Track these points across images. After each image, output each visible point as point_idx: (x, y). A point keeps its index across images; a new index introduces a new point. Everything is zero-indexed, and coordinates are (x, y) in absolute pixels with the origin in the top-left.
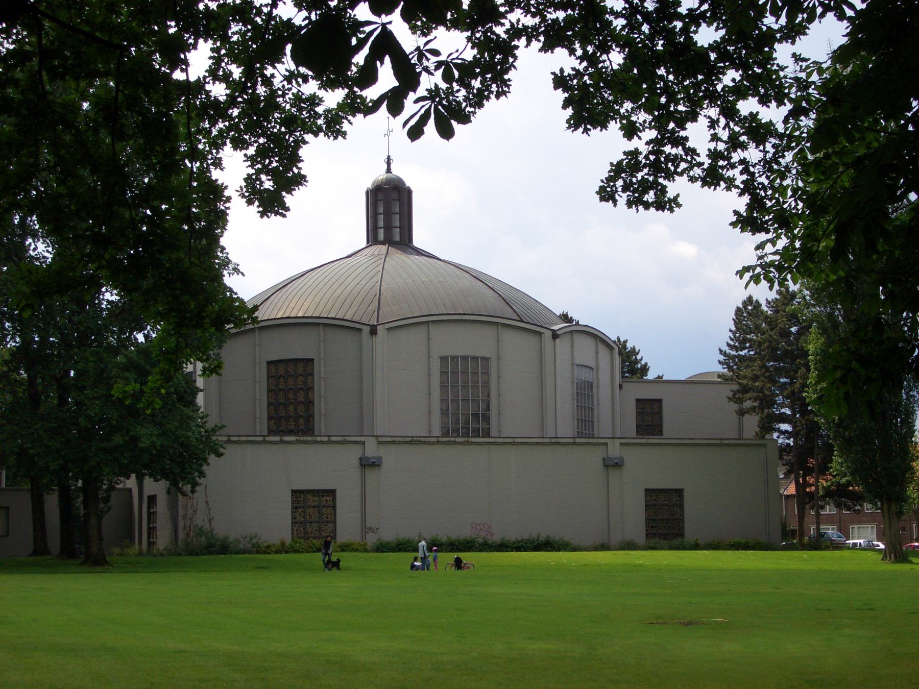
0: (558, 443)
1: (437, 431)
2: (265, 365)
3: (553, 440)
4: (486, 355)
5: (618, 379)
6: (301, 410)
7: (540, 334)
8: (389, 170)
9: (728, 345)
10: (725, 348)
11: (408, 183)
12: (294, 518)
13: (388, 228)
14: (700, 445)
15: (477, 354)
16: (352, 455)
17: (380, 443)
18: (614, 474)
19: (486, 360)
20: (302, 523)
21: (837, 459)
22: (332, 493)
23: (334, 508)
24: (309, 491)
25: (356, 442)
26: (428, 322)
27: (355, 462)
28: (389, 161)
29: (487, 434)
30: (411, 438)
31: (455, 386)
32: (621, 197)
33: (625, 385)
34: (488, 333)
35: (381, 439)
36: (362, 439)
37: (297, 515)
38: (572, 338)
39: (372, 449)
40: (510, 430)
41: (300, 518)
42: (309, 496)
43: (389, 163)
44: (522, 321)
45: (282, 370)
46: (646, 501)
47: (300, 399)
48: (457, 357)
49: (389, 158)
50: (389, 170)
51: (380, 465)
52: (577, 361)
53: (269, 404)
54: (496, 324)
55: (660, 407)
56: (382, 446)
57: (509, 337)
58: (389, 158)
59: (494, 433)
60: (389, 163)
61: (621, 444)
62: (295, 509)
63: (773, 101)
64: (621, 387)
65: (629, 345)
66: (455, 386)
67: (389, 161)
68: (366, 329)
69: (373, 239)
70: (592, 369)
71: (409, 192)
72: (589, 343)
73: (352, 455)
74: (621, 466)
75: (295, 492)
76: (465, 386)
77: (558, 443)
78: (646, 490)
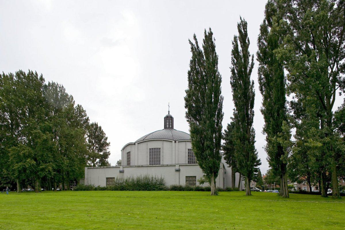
0: (163, 166)
1: (148, 164)
3: (162, 165)
7: (172, 142)
8: (169, 114)
11: (173, 116)
13: (169, 125)
14: (185, 165)
19: (160, 149)
24: (110, 178)
28: (169, 112)
29: (159, 164)
30: (104, 167)
32: (60, 85)
36: (120, 166)
40: (165, 163)
43: (169, 112)
45: (191, 179)
46: (186, 179)
48: (155, 148)
49: (169, 111)
50: (169, 114)
54: (185, 141)
57: (165, 143)
58: (169, 111)
59: (161, 163)
60: (169, 112)
62: (107, 182)
63: (334, 113)
67: (169, 112)
69: (165, 127)
74: (123, 172)
75: (107, 178)
77: (163, 166)
78: (186, 177)
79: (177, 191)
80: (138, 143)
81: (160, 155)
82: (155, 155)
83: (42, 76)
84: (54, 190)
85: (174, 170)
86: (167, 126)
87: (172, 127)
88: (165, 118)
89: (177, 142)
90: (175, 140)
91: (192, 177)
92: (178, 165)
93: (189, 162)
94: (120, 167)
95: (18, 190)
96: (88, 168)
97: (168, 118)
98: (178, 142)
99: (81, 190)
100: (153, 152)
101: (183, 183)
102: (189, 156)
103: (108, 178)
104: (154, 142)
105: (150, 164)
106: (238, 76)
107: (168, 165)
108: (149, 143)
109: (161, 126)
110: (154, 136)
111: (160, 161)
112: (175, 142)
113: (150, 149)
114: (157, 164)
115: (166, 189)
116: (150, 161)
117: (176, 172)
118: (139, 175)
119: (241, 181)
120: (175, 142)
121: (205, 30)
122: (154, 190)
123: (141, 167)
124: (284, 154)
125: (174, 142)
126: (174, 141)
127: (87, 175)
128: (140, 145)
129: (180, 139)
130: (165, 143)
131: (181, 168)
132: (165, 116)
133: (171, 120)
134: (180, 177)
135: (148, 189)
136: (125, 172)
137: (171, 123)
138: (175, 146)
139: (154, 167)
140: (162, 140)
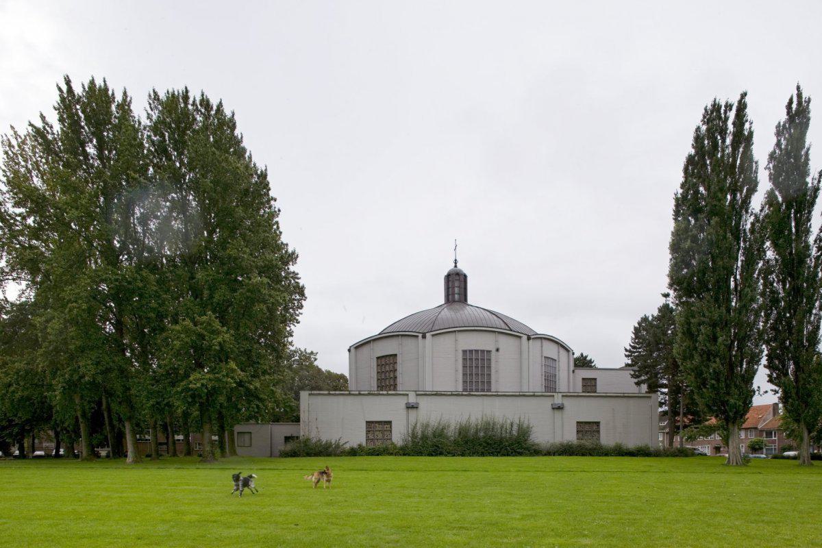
0: (524, 396)
1: (461, 389)
2: (375, 360)
4: (490, 349)
5: (572, 367)
6: (392, 383)
7: (520, 337)
8: (456, 266)
9: (630, 345)
10: (628, 348)
12: (367, 437)
15: (478, 348)
16: (401, 402)
17: (417, 395)
18: (557, 413)
20: (372, 439)
21: (748, 226)
22: (390, 423)
23: (391, 431)
25: (403, 395)
26: (455, 331)
27: (404, 406)
29: (489, 390)
31: (471, 367)
33: (576, 371)
34: (491, 337)
35: (418, 393)
37: (370, 435)
38: (542, 342)
39: (412, 399)
41: (371, 437)
42: (377, 425)
43: (456, 263)
44: (511, 330)
45: (587, 428)
47: (392, 376)
49: (456, 260)
50: (456, 266)
51: (417, 408)
52: (545, 355)
53: (378, 379)
55: (596, 383)
56: (418, 397)
58: (456, 260)
60: (456, 263)
61: (563, 396)
62: (368, 432)
64: (573, 371)
65: (588, 358)
66: (471, 367)
68: (420, 335)
70: (555, 360)
71: (465, 276)
72: (554, 347)
73: (401, 402)
74: (417, 408)
76: (477, 367)
78: (577, 422)
79: (576, 455)
81: (489, 367)
82: (477, 367)
84: (23, 456)
85: (550, 407)
89: (428, 335)
91: (589, 423)
92: (560, 395)
93: (378, 387)
94: (650, 397)
95: (130, 454)
96: (310, 395)
99: (308, 455)
101: (570, 436)
103: (373, 422)
104: (475, 334)
105: (465, 390)
106: (705, 190)
107: (536, 394)
108: (461, 337)
109: (436, 296)
111: (489, 383)
113: (464, 352)
115: (536, 451)
116: (465, 382)
117: (556, 411)
118: (463, 419)
120: (424, 337)
121: (83, 85)
122: (520, 454)
123: (449, 395)
125: (525, 337)
126: (526, 337)
127: (307, 414)
130: (409, 343)
131: (568, 403)
135: (503, 451)
136: (421, 406)
139: (430, 397)
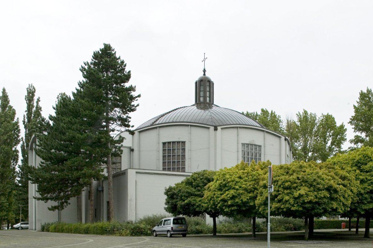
8: (204, 74)
19: (184, 143)
28: (204, 71)
48: (179, 142)
50: (204, 74)
54: (237, 127)
67: (204, 71)
80: (140, 132)
83: (126, 64)
86: (202, 99)
87: (210, 101)
88: (196, 83)
89: (219, 128)
90: (215, 125)
97: (202, 82)
98: (222, 129)
100: (169, 150)
102: (164, 157)
108: (163, 131)
110: (176, 118)
112: (216, 129)
113: (164, 144)
114: (174, 170)
119: (352, 233)
120: (216, 129)
124: (33, 101)
125: (212, 128)
128: (144, 135)
129: (235, 123)
132: (197, 78)
133: (210, 86)
134: (135, 217)
137: (208, 93)
138: (215, 135)
140: (188, 125)
